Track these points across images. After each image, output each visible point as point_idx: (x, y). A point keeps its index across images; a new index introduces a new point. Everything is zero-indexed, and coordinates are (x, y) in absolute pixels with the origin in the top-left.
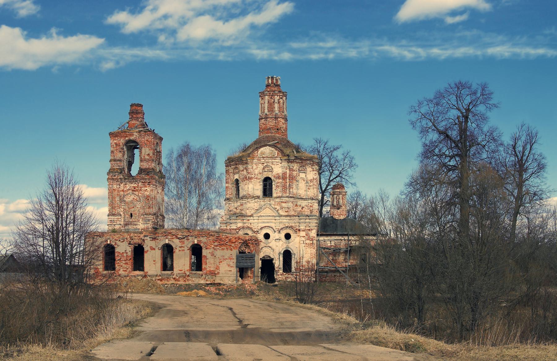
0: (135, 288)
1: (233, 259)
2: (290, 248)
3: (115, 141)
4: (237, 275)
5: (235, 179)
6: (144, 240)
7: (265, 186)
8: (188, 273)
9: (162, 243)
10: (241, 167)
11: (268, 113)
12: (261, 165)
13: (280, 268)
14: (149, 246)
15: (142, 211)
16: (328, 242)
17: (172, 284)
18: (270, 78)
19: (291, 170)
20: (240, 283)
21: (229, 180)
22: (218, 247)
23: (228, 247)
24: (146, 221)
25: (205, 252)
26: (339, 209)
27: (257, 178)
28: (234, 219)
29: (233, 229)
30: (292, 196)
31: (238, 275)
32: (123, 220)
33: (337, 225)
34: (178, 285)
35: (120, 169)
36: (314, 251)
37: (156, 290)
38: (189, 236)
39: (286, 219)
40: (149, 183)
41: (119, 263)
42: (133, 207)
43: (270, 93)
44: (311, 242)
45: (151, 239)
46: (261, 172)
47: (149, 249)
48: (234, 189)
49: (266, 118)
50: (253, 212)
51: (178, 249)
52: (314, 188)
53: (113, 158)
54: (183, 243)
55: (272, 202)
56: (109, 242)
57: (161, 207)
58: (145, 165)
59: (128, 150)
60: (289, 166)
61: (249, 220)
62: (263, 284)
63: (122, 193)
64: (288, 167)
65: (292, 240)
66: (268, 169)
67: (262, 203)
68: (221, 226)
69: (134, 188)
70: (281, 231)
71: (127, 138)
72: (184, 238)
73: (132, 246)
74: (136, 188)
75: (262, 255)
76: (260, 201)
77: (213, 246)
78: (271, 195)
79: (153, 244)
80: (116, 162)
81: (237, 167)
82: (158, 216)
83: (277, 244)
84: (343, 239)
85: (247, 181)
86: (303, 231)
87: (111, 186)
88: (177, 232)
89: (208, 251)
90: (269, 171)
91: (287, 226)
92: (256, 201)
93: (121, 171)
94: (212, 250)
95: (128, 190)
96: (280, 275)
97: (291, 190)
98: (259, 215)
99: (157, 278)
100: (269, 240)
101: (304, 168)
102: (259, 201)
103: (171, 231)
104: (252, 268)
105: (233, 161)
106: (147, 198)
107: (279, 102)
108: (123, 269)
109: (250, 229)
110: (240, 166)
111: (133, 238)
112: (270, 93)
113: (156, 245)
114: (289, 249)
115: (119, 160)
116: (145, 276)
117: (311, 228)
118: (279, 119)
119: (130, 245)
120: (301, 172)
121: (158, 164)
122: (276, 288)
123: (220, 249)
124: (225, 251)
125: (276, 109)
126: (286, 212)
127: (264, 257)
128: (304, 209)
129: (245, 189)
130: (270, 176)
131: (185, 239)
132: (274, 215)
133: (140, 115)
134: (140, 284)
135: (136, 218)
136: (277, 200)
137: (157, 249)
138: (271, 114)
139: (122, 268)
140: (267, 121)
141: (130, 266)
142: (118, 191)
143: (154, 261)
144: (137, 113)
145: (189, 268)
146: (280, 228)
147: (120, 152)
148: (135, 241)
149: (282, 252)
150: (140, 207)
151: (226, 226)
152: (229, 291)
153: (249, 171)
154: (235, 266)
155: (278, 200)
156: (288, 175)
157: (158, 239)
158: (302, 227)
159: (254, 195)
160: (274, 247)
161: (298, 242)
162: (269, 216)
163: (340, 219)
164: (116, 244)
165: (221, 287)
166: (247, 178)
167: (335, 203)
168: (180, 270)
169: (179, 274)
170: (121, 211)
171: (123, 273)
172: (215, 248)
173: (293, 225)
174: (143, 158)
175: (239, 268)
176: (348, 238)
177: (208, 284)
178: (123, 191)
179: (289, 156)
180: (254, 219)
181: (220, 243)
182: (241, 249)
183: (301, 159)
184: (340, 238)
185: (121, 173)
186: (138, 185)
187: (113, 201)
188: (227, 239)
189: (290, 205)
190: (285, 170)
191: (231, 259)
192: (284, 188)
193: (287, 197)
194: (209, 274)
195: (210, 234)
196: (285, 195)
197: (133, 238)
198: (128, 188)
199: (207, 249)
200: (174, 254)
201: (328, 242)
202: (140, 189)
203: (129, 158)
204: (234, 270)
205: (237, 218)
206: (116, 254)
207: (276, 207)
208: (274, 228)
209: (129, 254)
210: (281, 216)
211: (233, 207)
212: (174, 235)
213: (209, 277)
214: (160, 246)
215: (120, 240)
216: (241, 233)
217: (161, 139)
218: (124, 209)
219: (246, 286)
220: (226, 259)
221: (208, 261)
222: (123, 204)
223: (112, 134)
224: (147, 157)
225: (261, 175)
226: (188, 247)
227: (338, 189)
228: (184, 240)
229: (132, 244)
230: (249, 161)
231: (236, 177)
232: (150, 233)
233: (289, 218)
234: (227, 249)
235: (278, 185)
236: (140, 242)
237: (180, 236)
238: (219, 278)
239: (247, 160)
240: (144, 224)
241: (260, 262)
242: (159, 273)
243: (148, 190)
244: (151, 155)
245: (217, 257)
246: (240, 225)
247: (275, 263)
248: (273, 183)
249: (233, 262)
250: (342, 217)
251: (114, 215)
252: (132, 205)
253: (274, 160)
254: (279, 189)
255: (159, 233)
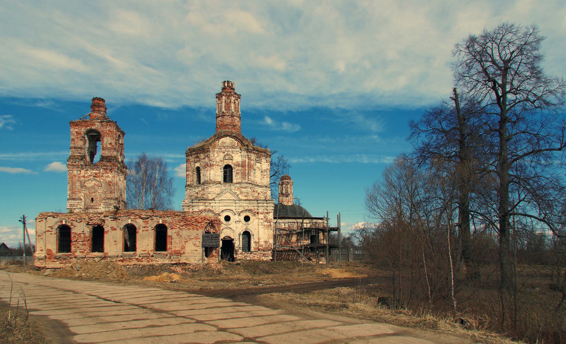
0: (90, 271)
1: (199, 239)
2: (250, 230)
3: (76, 130)
4: (203, 255)
5: (196, 166)
6: (104, 221)
7: (225, 173)
8: (152, 254)
9: (125, 223)
10: (202, 156)
11: (225, 112)
12: (222, 153)
13: (240, 248)
14: (110, 227)
15: (103, 196)
16: (282, 225)
17: (134, 265)
18: (226, 82)
19: (249, 159)
20: (206, 262)
21: (190, 169)
22: (184, 227)
23: (194, 227)
24: (107, 205)
25: (169, 232)
26: (287, 196)
27: (218, 165)
28: (197, 203)
29: (195, 212)
30: (250, 182)
31: (204, 255)
32: (83, 204)
33: (287, 210)
34: (141, 266)
35: (81, 156)
36: (271, 232)
37: (116, 274)
38: (153, 216)
39: (246, 203)
40: (111, 170)
41: (75, 244)
42: (95, 192)
43: (227, 94)
44: (269, 224)
45: (112, 219)
46: (222, 159)
47: (110, 229)
48: (195, 176)
49: (223, 116)
50: (214, 196)
51: (142, 229)
52: (267, 177)
53: (73, 146)
54: (147, 223)
55: (233, 188)
56: (64, 223)
57: (123, 194)
58: (107, 153)
59: (89, 139)
60: (248, 155)
61: (210, 203)
62: (227, 263)
63: (83, 179)
64: (247, 156)
65: (251, 222)
66: (229, 157)
67: (223, 188)
68: (183, 209)
69: (96, 174)
70: (241, 214)
71: (88, 128)
72: (148, 218)
73: (91, 227)
74: (98, 174)
75: (222, 236)
76: (221, 186)
77: (178, 226)
78: (231, 181)
79: (114, 224)
80: (76, 150)
81: (198, 156)
82: (119, 201)
83: (238, 225)
84: (296, 221)
85: (209, 168)
86: (261, 214)
87: (71, 172)
88: (141, 212)
89: (174, 231)
90: (229, 159)
91: (246, 209)
92: (217, 186)
93: (83, 158)
94: (178, 229)
95: (89, 176)
96: (240, 255)
97: (250, 177)
98: (220, 199)
99: (119, 259)
100: (230, 222)
101: (260, 159)
102: (220, 186)
103: (135, 211)
104: (217, 247)
105: (194, 151)
106: (109, 184)
107: (235, 103)
108: (80, 250)
109: (212, 211)
110: (201, 155)
111: (92, 218)
112: (227, 94)
113: (117, 225)
114: (249, 231)
115: (79, 148)
116: (105, 257)
117: (269, 211)
118: (235, 117)
119: (88, 226)
120: (257, 162)
121: (120, 155)
122: (239, 266)
123: (186, 228)
124: (191, 230)
125: (233, 108)
126: (245, 196)
127: (224, 238)
128: (260, 195)
129: (207, 175)
130: (230, 164)
131: (149, 219)
132: (235, 199)
133: (102, 109)
134: (97, 266)
135: (97, 202)
136: (237, 186)
137: (118, 229)
138: (228, 112)
139: (79, 249)
140: (224, 118)
141: (87, 247)
142: (79, 177)
143: (115, 241)
144: (99, 106)
145: (153, 249)
146: (240, 211)
147: (81, 140)
148: (94, 221)
149: (242, 233)
150: (101, 191)
151: (189, 209)
152: (196, 271)
153: (211, 158)
154: (201, 245)
155: (238, 185)
156: (247, 163)
157: (120, 219)
158: (261, 210)
159: (216, 181)
160: (234, 228)
161: (257, 223)
162: (230, 200)
163: (289, 206)
164: (72, 224)
165: (187, 267)
166: (209, 165)
167: (284, 192)
168: (144, 251)
169: (142, 254)
170: (82, 195)
171: (80, 254)
172: (181, 227)
173: (252, 208)
174: (105, 146)
175: (205, 248)
176: (303, 221)
177: (174, 264)
178: (84, 177)
179: (248, 146)
180: (215, 203)
181: (186, 223)
182: (207, 229)
183: (258, 150)
184: (293, 220)
185: (82, 159)
186: (100, 172)
187: (74, 186)
188: (193, 219)
189: (249, 190)
190: (244, 159)
191: (197, 239)
192: (244, 175)
193: (246, 183)
194: (175, 254)
195: (176, 214)
196: (244, 181)
197: (92, 218)
198: (90, 174)
199: (172, 229)
200: (137, 235)
201: (282, 225)
202: (101, 175)
203: (91, 149)
204: (200, 250)
205: (199, 201)
206: (72, 235)
207: (236, 191)
208: (235, 211)
209: (87, 235)
210: (241, 200)
211: (194, 193)
212: (137, 215)
213: (175, 257)
214: (122, 227)
215: (77, 221)
216: (204, 214)
217: (123, 133)
218: (85, 194)
219: (212, 265)
220: (192, 239)
221: (173, 241)
222: (84, 189)
223: (72, 123)
224: (109, 146)
225: (222, 162)
226: (152, 227)
227: (286, 179)
228: (148, 220)
229: (90, 225)
230: (211, 149)
231: (197, 165)
232: (111, 213)
233: (249, 202)
234: (193, 228)
235: (238, 172)
236: (100, 223)
237: (144, 216)
238: (185, 258)
239: (209, 148)
240: (105, 208)
241: (221, 242)
242: (120, 254)
243: (110, 176)
244: (113, 144)
245: (182, 236)
246: (202, 208)
247: (235, 243)
248: (233, 170)
249: (200, 242)
250: (290, 204)
251: (74, 199)
252: (93, 190)
253: (234, 150)
254: (239, 176)
255: (121, 213)
